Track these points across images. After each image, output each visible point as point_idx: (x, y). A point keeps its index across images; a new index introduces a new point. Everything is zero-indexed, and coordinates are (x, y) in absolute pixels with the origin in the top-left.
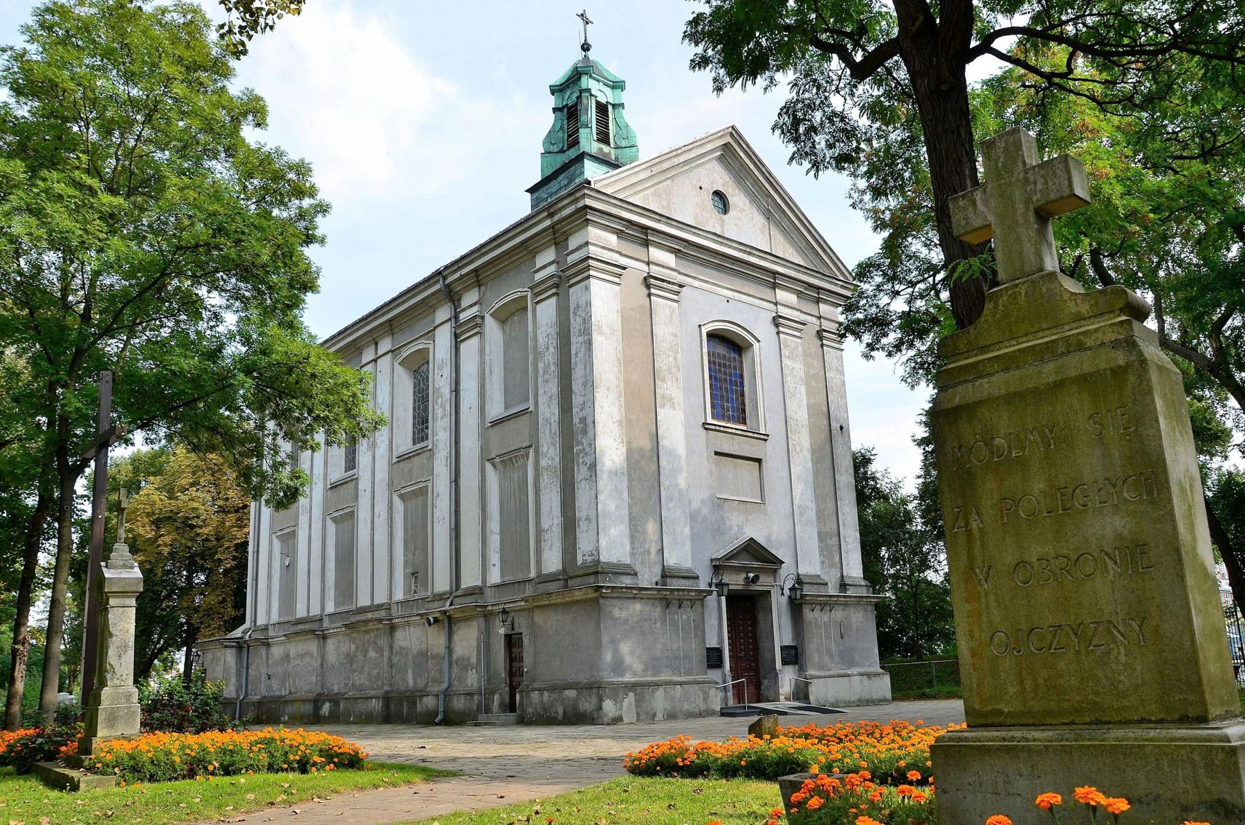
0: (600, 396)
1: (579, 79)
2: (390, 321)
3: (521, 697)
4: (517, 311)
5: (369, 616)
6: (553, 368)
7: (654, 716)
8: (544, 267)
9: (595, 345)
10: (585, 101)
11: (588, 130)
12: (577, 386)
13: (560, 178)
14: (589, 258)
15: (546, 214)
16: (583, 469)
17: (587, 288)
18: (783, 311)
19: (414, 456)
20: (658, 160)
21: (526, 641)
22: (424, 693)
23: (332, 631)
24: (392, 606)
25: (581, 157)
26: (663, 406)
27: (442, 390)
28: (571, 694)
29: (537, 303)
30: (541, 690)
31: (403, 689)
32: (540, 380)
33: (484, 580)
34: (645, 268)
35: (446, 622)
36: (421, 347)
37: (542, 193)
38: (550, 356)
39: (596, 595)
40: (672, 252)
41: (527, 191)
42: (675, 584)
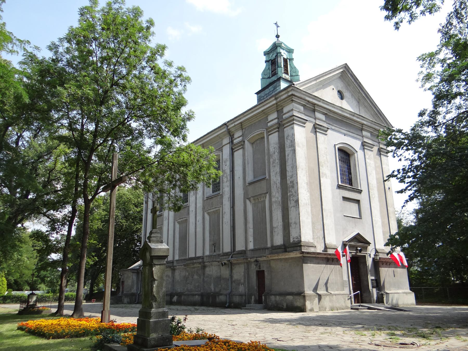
0: (299, 172)
1: (277, 48)
3: (265, 298)
4: (259, 139)
5: (195, 261)
6: (277, 161)
7: (326, 308)
8: (272, 120)
9: (297, 151)
10: (279, 57)
11: (281, 69)
12: (289, 168)
13: (270, 88)
15: (274, 98)
17: (293, 128)
18: (365, 140)
19: (214, 197)
20: (319, 77)
21: (266, 274)
22: (219, 294)
24: (204, 257)
25: (279, 79)
26: (323, 177)
28: (290, 298)
29: (269, 135)
30: (275, 295)
31: (209, 291)
32: (271, 166)
33: (246, 247)
35: (230, 265)
37: (262, 94)
38: (276, 156)
40: (324, 114)
41: (255, 93)
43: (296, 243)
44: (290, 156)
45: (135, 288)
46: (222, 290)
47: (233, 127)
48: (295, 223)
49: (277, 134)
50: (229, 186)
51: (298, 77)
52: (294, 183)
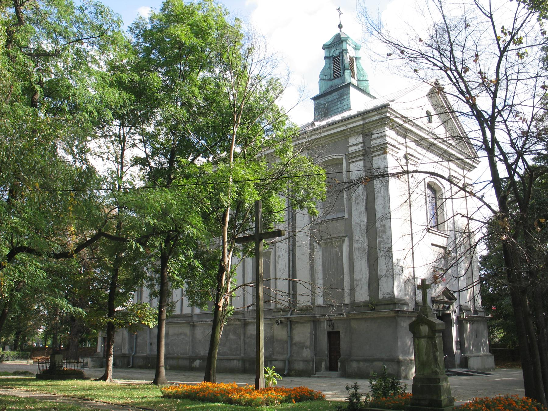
13: (334, 94)
14: (387, 143)
15: (360, 118)
17: (385, 159)
21: (342, 335)
23: (200, 323)
33: (313, 303)
35: (289, 323)
37: (322, 101)
43: (386, 300)
45: (127, 347)
46: (275, 354)
49: (362, 163)
51: (367, 82)
52: (386, 227)
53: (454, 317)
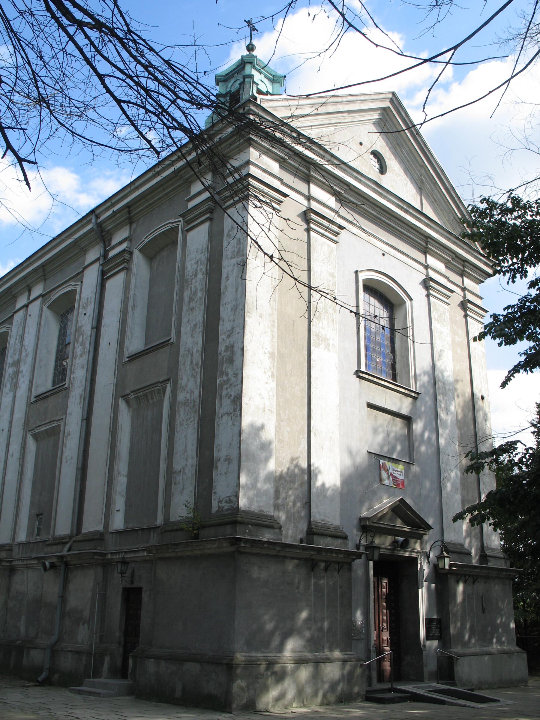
1: (244, 67)
2: (43, 266)
3: (135, 663)
6: (200, 294)
10: (247, 86)
12: (225, 312)
16: (226, 402)
19: (51, 395)
21: (145, 597)
26: (318, 346)
27: (84, 328)
28: (193, 668)
30: (158, 658)
32: (185, 308)
34: (305, 203)
36: (69, 289)
39: (232, 549)
42: (322, 543)
44: (232, 279)
47: (110, 217)
48: (228, 460)
50: (86, 367)
53: (425, 568)
